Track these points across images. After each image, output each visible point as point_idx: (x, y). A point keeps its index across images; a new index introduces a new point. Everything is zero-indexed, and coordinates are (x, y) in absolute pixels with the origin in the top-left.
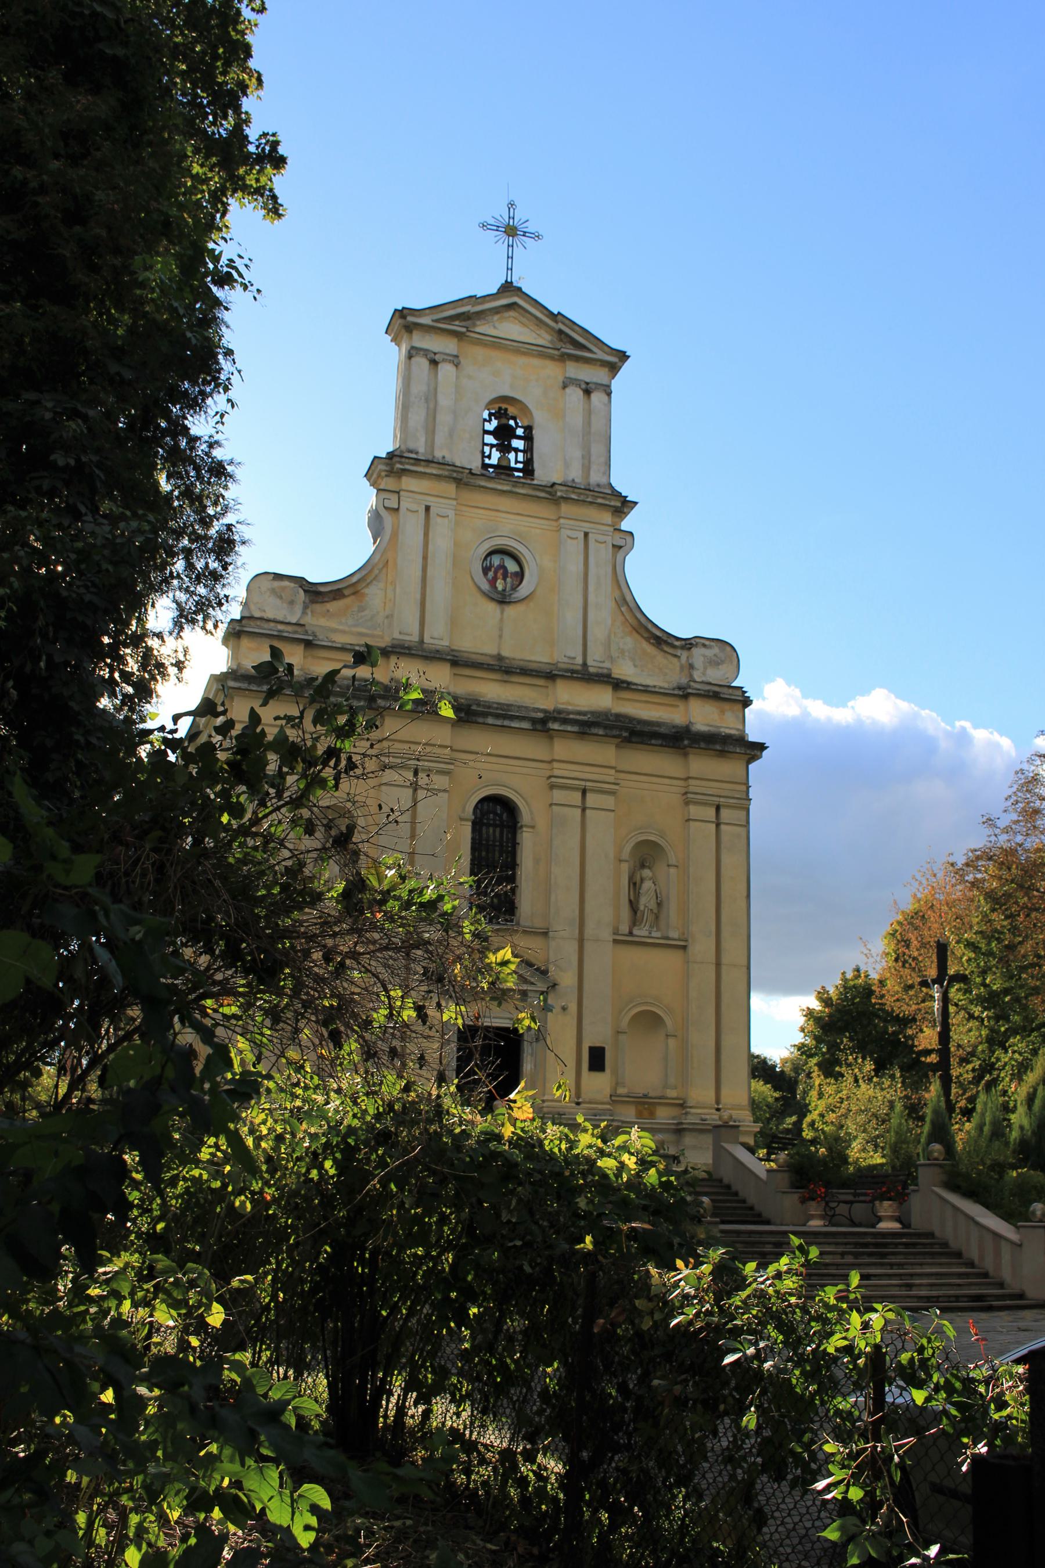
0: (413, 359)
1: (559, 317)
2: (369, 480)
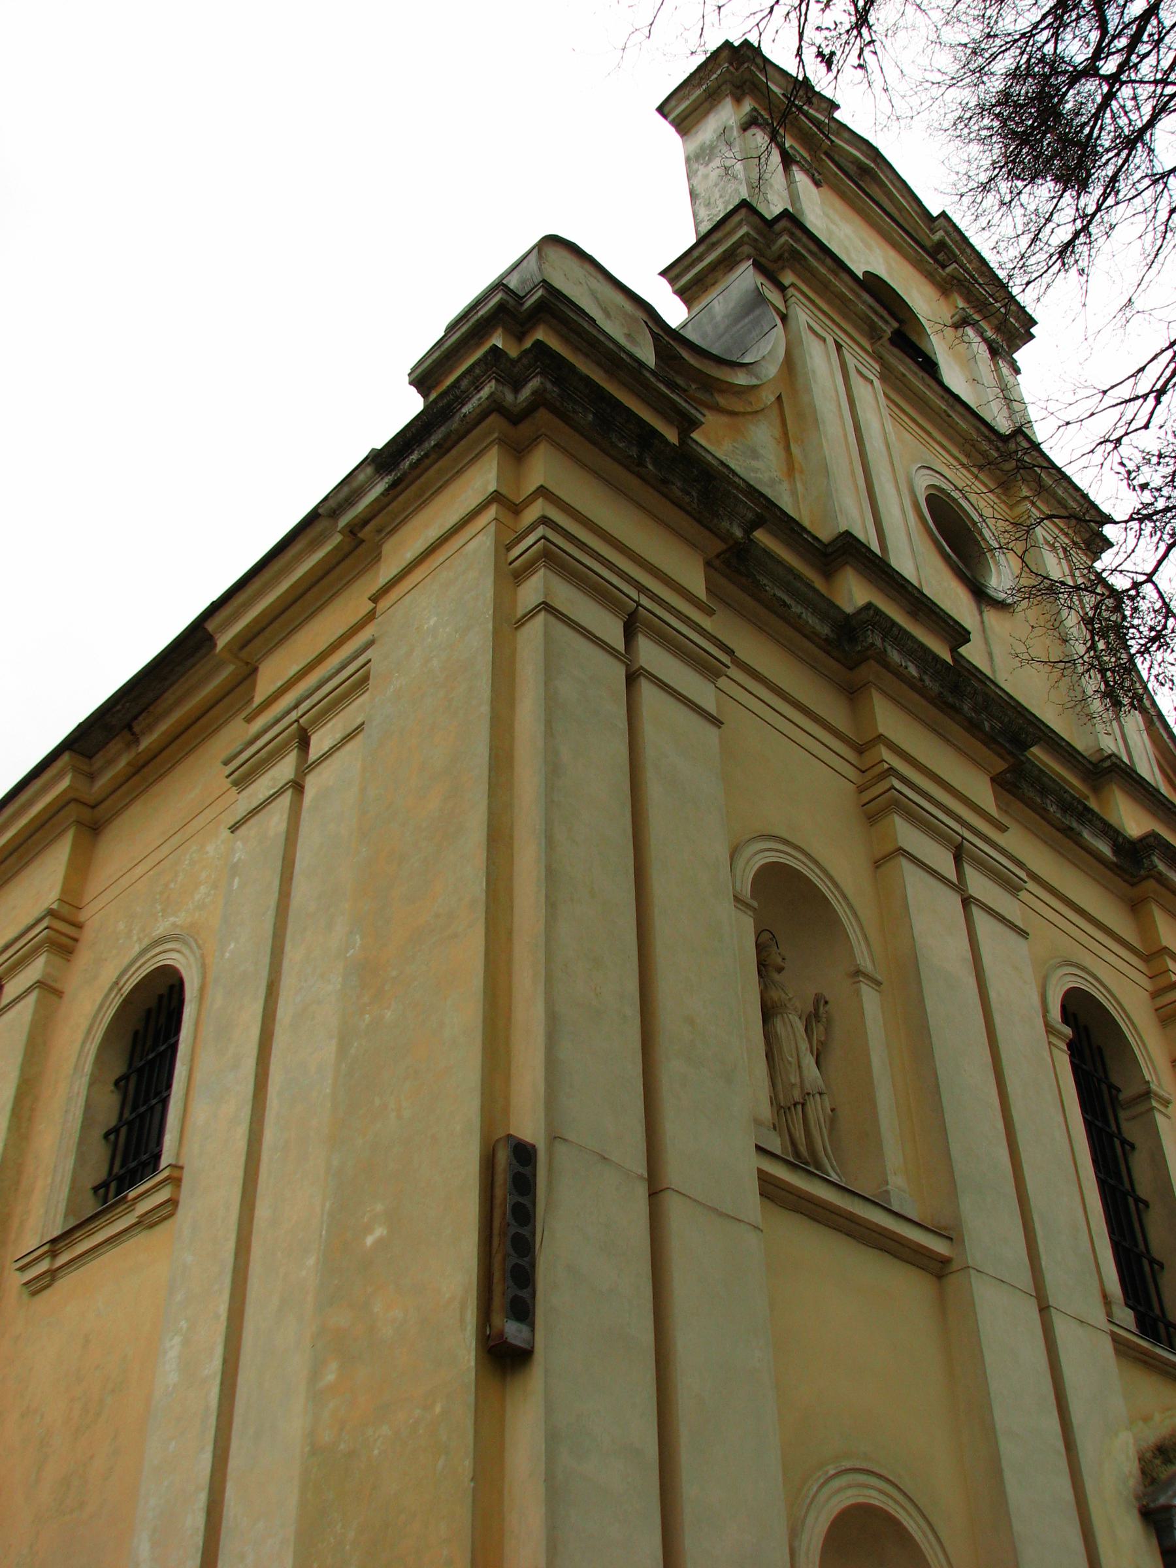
0: (754, 130)
1: (942, 220)
2: (672, 282)
